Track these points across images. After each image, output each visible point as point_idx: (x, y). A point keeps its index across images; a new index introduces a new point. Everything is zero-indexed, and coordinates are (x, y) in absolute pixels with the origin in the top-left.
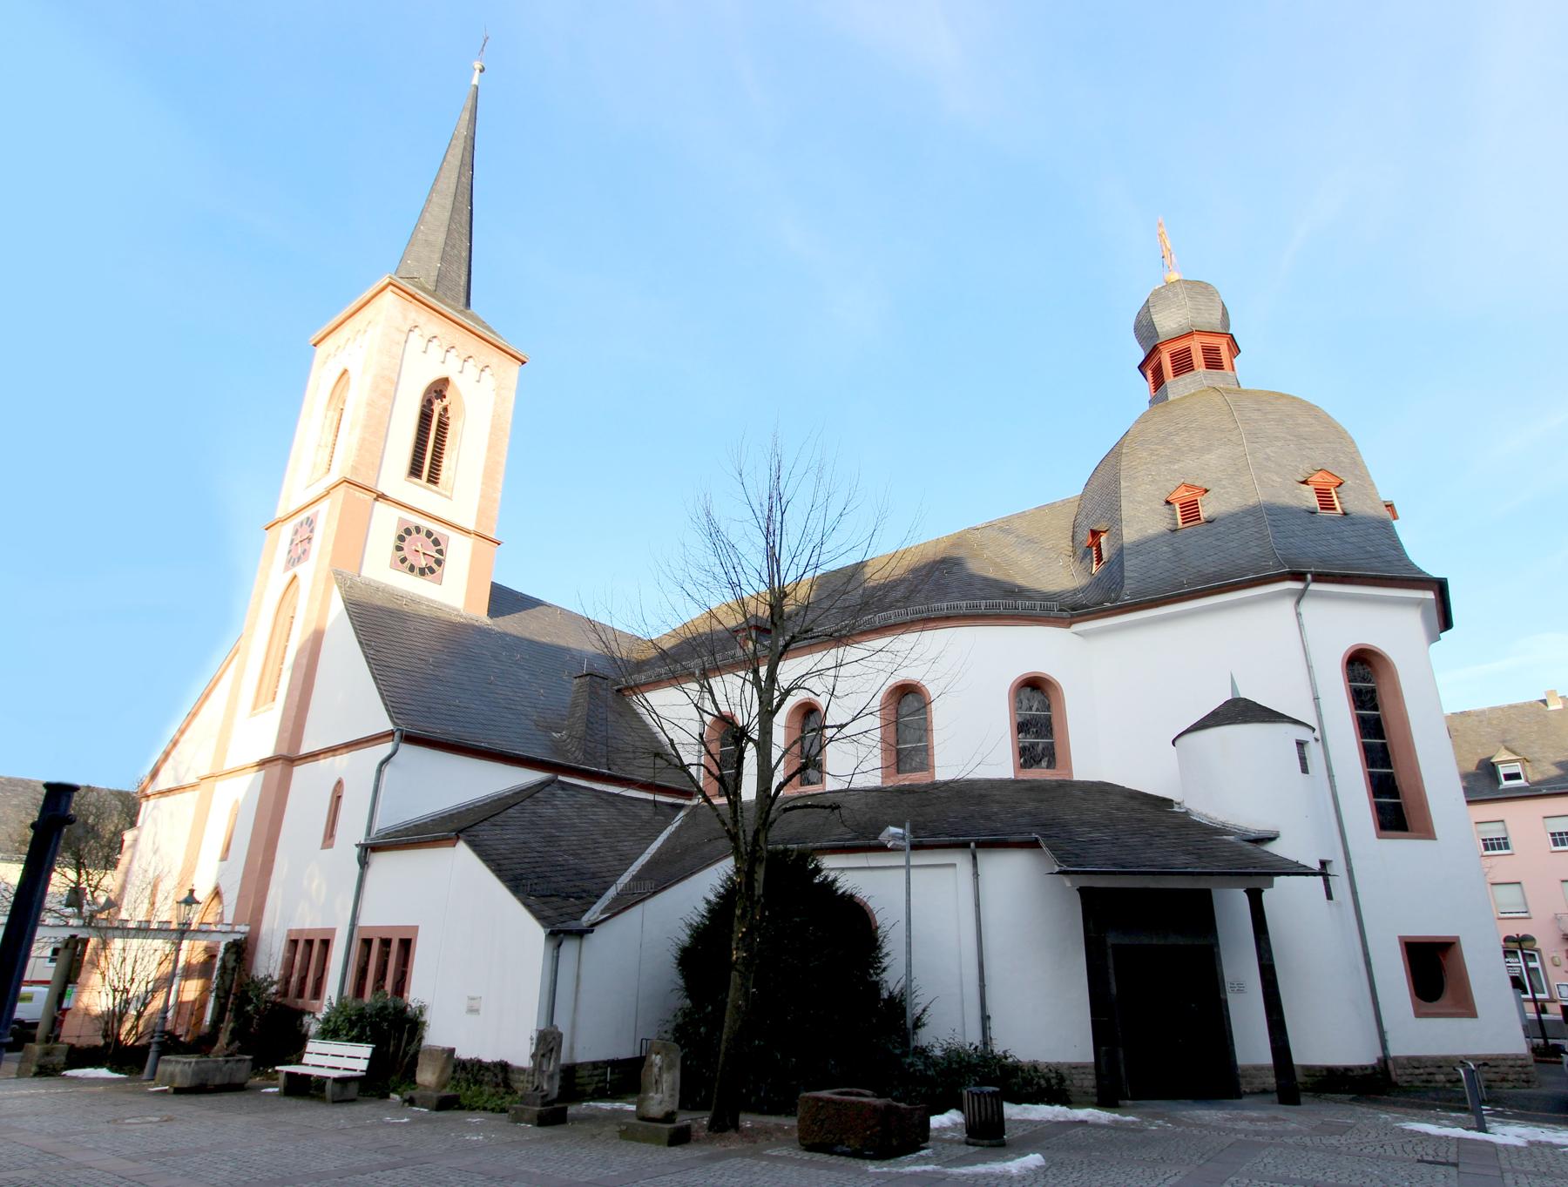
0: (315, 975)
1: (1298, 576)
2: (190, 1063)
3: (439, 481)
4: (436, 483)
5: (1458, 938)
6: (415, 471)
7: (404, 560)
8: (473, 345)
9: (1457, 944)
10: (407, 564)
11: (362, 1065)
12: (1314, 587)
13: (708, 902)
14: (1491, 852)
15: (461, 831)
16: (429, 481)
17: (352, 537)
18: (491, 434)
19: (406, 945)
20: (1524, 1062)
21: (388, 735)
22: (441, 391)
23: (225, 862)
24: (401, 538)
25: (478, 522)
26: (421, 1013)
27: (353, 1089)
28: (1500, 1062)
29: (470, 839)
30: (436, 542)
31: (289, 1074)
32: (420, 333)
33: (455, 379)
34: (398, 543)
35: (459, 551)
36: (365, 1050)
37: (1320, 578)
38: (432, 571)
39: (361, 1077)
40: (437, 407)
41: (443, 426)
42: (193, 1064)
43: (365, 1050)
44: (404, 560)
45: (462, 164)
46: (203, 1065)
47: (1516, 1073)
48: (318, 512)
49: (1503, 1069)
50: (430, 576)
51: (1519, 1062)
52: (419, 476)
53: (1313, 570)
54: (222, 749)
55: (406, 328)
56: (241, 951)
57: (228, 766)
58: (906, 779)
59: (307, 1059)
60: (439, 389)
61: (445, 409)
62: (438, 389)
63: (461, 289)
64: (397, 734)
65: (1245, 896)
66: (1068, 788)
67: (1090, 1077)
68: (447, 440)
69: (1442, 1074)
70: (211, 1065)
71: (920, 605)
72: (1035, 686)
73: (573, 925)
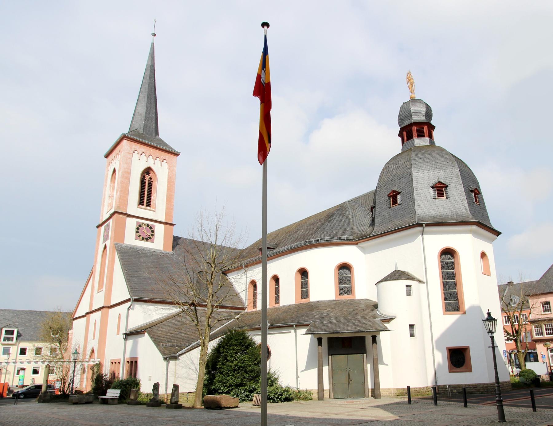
0: (134, 372)
1: (421, 225)
2: (76, 396)
3: (151, 205)
4: (150, 206)
5: (469, 347)
6: (141, 203)
7: (139, 236)
8: (158, 153)
9: (468, 349)
10: (141, 237)
11: (118, 395)
12: (427, 229)
13: (214, 347)
14: (545, 313)
15: (146, 329)
16: (147, 206)
17: (120, 231)
18: (168, 185)
19: (136, 362)
20: (487, 386)
21: (128, 300)
22: (148, 172)
23: (118, 335)
24: (138, 229)
25: (166, 218)
26: (140, 381)
27: (116, 401)
28: (477, 386)
29: (149, 331)
30: (151, 228)
31: (102, 398)
32: (137, 153)
33: (153, 167)
34: (137, 230)
35: (159, 229)
36: (119, 391)
37: (428, 225)
38: (150, 238)
39: (118, 398)
40: (147, 178)
41: (150, 185)
42: (77, 397)
43: (119, 391)
44: (139, 236)
45: (150, 78)
46: (80, 397)
47: (483, 389)
48: (110, 222)
49: (478, 388)
50: (150, 240)
51: (485, 386)
52: (143, 205)
53: (425, 222)
54: (91, 305)
55: (132, 152)
56: (99, 365)
57: (94, 309)
58: (305, 301)
59: (107, 394)
60: (148, 171)
61: (151, 178)
62: (147, 171)
63: (153, 130)
64: (132, 299)
65: (371, 338)
66: (353, 302)
67: (192, 382)
68: (152, 190)
69: (456, 390)
70: (82, 397)
71: (307, 240)
72: (345, 267)
73: (173, 355)
